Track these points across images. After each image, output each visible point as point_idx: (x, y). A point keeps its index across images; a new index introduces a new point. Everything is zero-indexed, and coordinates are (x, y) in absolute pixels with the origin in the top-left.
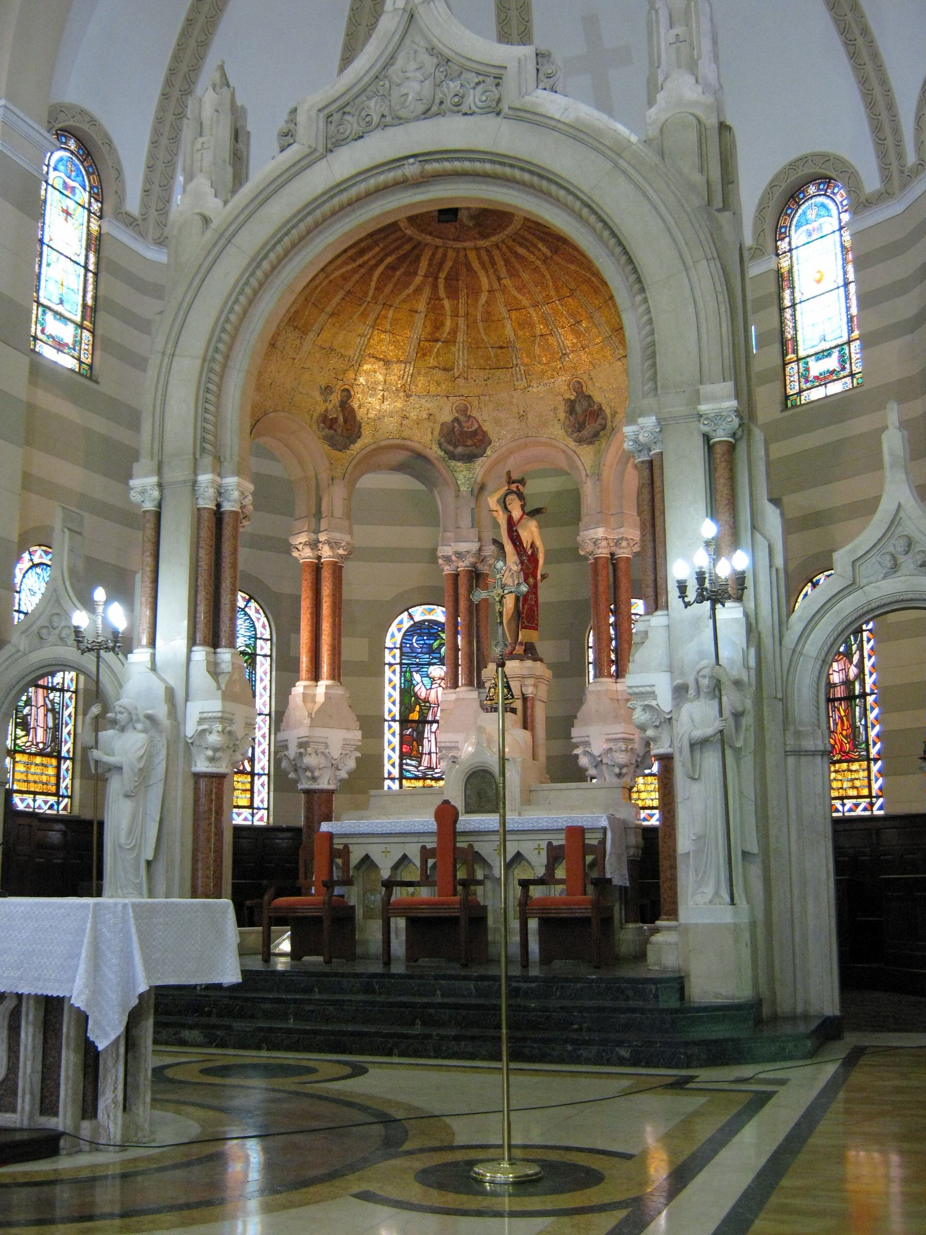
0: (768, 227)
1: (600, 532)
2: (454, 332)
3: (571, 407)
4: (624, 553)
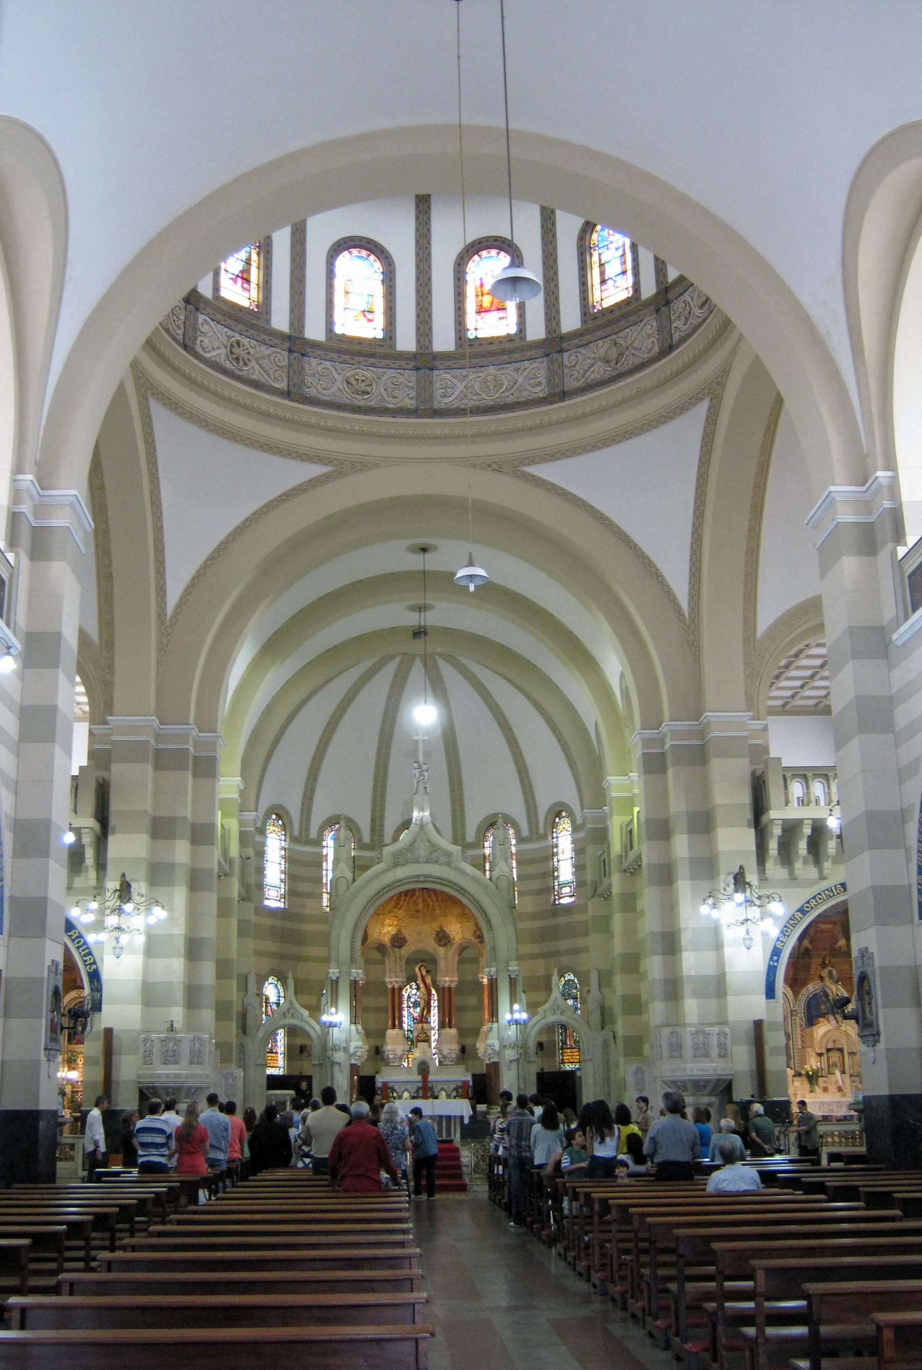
0: (482, 836)
1: (447, 979)
2: (402, 906)
3: (438, 933)
4: (453, 985)
